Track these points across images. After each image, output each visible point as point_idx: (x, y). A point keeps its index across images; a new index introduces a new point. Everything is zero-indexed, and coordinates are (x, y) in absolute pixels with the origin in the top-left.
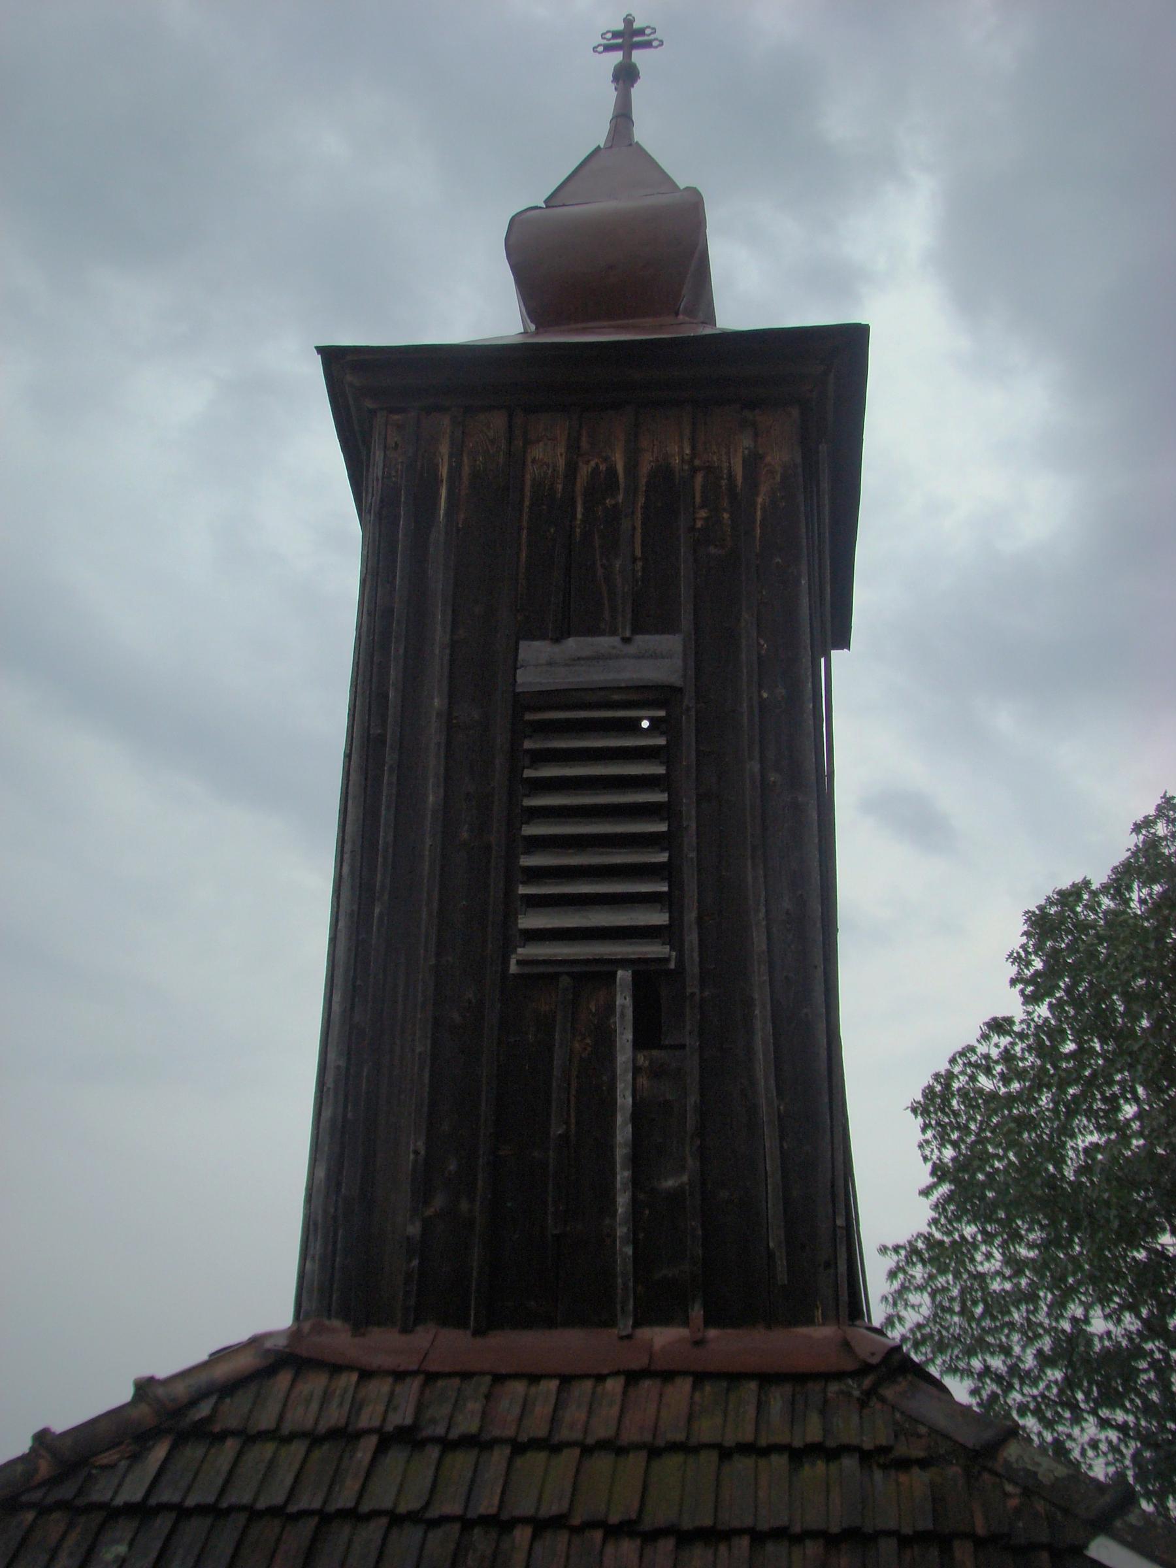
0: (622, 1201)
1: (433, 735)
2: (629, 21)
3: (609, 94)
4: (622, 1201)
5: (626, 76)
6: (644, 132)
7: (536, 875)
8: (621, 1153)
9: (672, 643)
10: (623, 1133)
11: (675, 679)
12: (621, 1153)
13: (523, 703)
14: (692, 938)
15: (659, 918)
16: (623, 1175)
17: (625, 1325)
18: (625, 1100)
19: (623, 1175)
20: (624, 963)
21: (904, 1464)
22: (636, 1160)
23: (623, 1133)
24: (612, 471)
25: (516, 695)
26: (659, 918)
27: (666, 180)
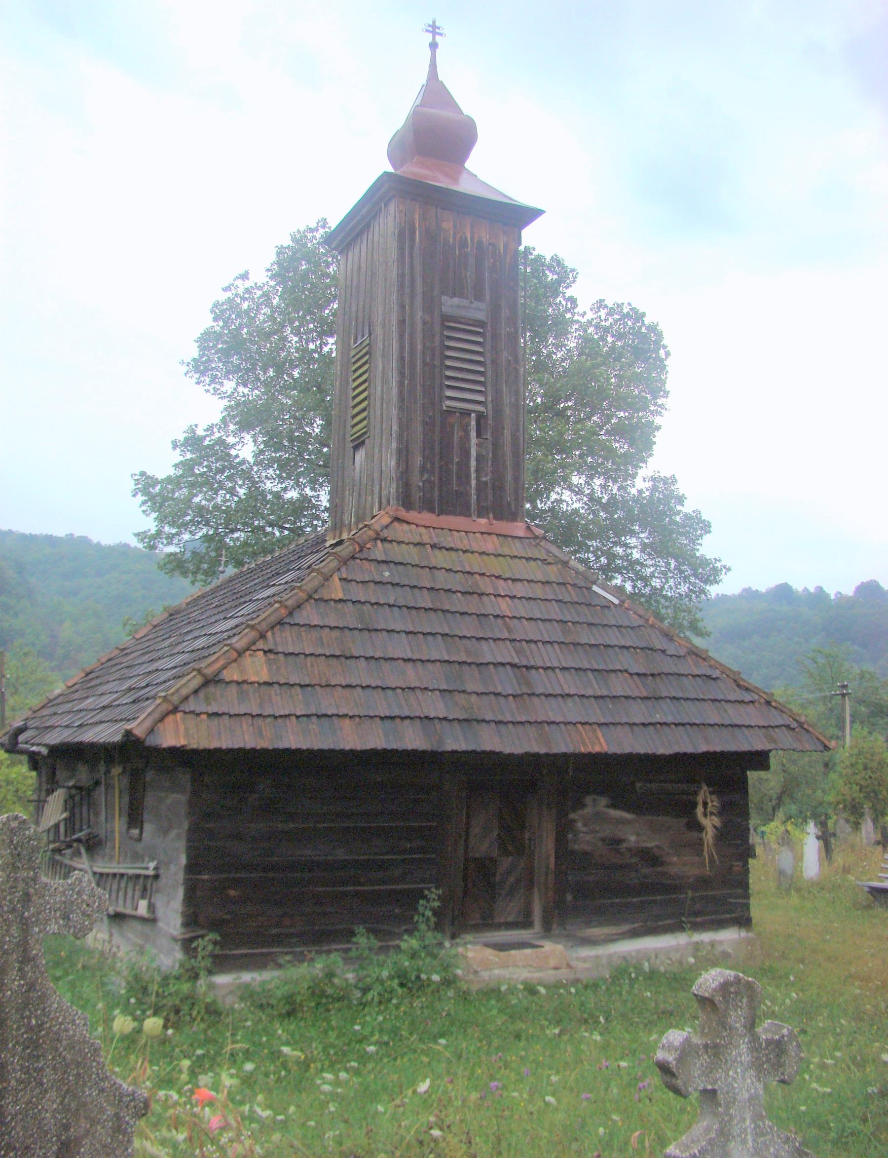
0: (473, 483)
1: (419, 326)
2: (434, 22)
3: (428, 53)
4: (473, 483)
5: (434, 46)
6: (441, 77)
7: (449, 378)
8: (473, 469)
9: (482, 306)
10: (473, 463)
11: (484, 319)
12: (473, 469)
13: (445, 318)
14: (490, 406)
15: (448, 363)
16: (473, 476)
17: (474, 518)
18: (473, 453)
19: (473, 476)
20: (474, 411)
21: (550, 564)
22: (477, 471)
23: (473, 463)
24: (466, 239)
25: (442, 316)
26: (448, 363)
27: (461, 113)
